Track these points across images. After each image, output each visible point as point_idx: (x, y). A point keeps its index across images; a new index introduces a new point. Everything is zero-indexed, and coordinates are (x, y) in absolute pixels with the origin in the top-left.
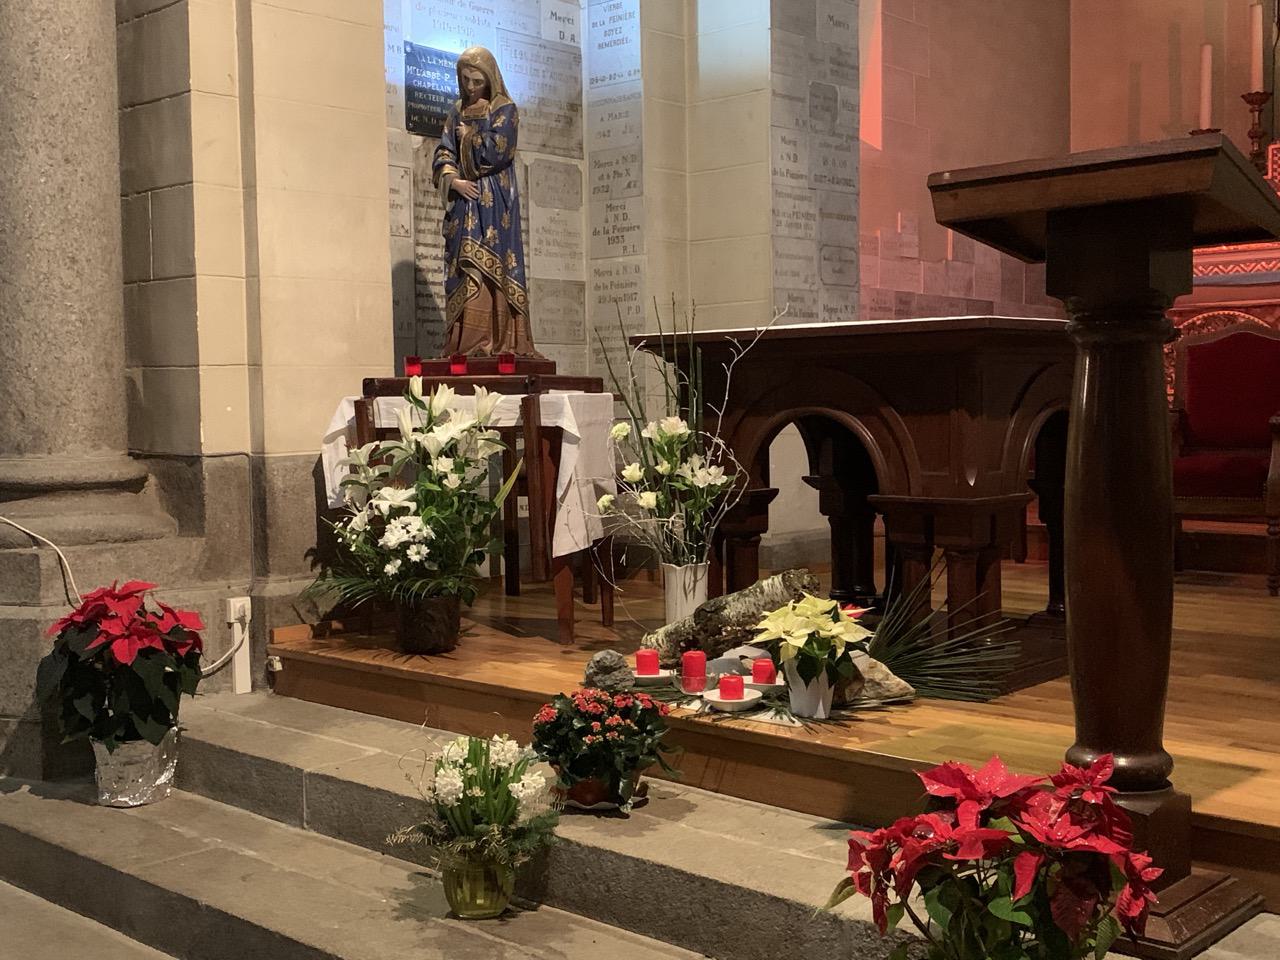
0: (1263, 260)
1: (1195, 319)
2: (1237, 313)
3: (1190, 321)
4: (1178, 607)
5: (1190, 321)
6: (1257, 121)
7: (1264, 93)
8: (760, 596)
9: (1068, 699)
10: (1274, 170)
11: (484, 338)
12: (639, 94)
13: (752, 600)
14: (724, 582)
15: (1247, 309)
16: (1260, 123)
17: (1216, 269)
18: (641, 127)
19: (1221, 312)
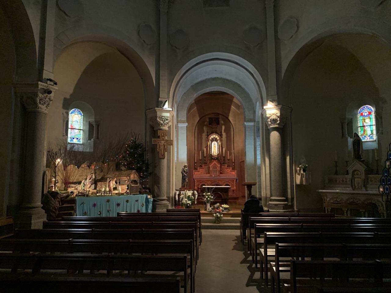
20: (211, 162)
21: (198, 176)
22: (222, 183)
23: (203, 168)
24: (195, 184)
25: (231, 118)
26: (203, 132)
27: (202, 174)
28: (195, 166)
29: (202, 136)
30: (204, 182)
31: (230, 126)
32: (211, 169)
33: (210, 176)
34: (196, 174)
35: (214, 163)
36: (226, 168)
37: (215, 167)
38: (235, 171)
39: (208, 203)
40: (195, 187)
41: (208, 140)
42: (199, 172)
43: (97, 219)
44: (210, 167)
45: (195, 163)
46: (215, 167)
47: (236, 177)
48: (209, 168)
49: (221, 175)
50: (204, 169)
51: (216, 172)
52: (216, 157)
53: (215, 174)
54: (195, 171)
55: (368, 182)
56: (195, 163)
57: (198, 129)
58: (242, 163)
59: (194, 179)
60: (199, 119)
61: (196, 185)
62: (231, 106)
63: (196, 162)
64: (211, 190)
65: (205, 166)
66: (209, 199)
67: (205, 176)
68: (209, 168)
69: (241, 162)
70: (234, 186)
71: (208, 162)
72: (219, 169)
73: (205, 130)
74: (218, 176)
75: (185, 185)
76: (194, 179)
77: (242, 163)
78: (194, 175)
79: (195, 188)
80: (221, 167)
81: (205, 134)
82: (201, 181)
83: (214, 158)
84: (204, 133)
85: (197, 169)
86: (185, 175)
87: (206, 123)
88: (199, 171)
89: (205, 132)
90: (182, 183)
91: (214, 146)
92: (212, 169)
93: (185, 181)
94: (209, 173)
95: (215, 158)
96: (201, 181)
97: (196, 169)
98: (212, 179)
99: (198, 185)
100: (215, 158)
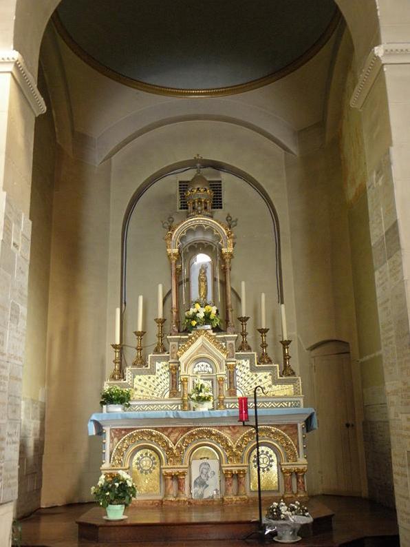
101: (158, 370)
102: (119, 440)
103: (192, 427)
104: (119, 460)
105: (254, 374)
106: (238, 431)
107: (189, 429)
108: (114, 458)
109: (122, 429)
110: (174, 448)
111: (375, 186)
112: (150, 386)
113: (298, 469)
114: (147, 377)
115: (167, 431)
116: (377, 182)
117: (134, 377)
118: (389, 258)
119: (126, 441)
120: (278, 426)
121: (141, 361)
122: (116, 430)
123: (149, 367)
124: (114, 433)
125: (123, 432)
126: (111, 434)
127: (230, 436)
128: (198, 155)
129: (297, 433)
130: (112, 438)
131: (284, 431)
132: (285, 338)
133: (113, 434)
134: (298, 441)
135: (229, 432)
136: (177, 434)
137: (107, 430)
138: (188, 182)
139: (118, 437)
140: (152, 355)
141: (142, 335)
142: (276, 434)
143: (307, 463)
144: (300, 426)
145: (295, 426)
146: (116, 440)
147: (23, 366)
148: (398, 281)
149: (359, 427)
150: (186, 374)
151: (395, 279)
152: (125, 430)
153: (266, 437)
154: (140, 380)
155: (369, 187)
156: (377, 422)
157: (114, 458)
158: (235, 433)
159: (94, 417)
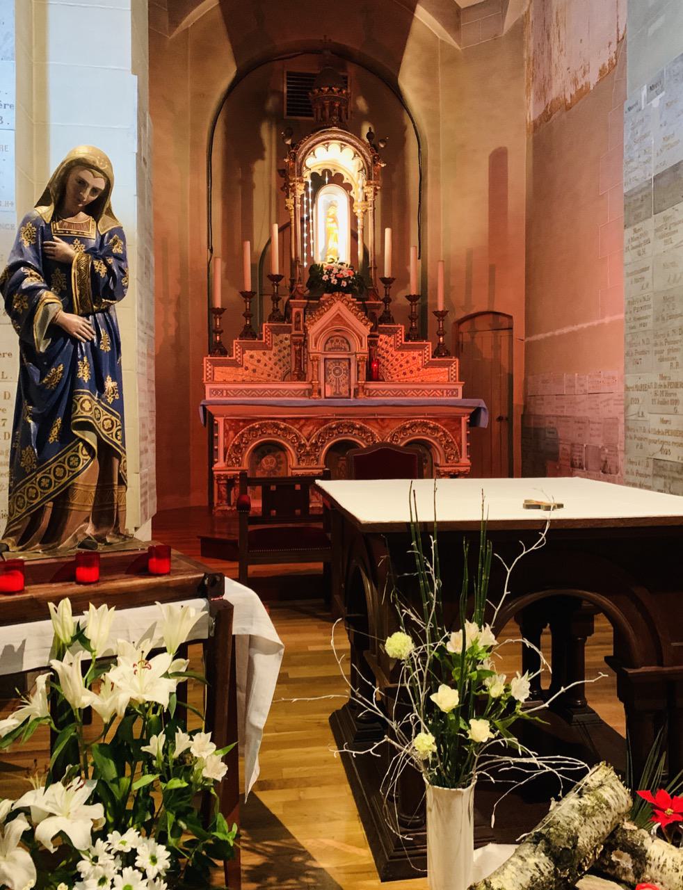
0: (269, 389)
1: (254, 424)
2: (279, 422)
3: (251, 426)
4: (588, 650)
5: (251, 426)
6: (248, 307)
7: (251, 292)
8: (607, 812)
9: (321, 742)
10: (266, 338)
11: (87, 520)
12: (13, 226)
13: (600, 818)
14: (360, 782)
15: (284, 420)
16: (249, 309)
17: (412, 392)
18: (660, 212)
19: (270, 421)
20: (313, 309)
21: (237, 392)
22: (389, 431)
23: (265, 347)
24: (212, 440)
25: (410, 83)
26: (259, 153)
27: (259, 382)
28: (212, 331)
29: (248, 172)
30: (277, 426)
31: (404, 128)
32: (315, 348)
33: (310, 392)
34: (218, 377)
35: (329, 315)
36: (401, 348)
37: (338, 336)
38: (448, 364)
39: (452, 779)
40: (212, 463)
41: (286, 188)
42: (240, 370)
43: (207, 420)
44: (306, 335)
45: (213, 312)
46: (338, 336)
47: (460, 396)
48: (301, 344)
49: (372, 386)
50: (270, 353)
51: (343, 366)
52: (345, 273)
53: (338, 381)
54: (215, 364)
55: (553, 428)
56: (213, 312)
57: (227, 123)
58: (465, 327)
59: (205, 410)
60: (231, 72)
61: (220, 447)
62: (413, 10)
63: (218, 304)
64: (497, 571)
65: (277, 331)
66: (480, 730)
67: (276, 393)
68: (304, 344)
69: (460, 322)
70: (458, 454)
71: (295, 310)
72: (360, 348)
73: (266, 144)
74: (356, 392)
75: (63, 500)
76: (205, 410)
77: (464, 324)
78: (208, 387)
79: (216, 466)
80: (372, 343)
81: (266, 162)
82: (254, 420)
83: (334, 281)
84: (263, 158)
85: (224, 352)
86: (57, 331)
87: (270, 104)
88: (235, 364)
89: (267, 154)
90: (18, 472)
91: (327, 215)
92: (320, 348)
93: (67, 437)
94: (301, 376)
95: (339, 280)
96: (254, 420)
97: (218, 350)
98: (328, 413)
99: (237, 448)
100: (339, 280)
101: (402, 355)
102: (236, 434)
103: (330, 419)
104: (236, 458)
105: (400, 353)
106: (387, 426)
107: (327, 421)
108: (230, 455)
109: (240, 420)
110: (308, 444)
111: (643, 108)
112: (265, 365)
113: (459, 472)
114: (261, 352)
115: (298, 423)
116: (649, 100)
117: (244, 352)
118: (655, 214)
119: (245, 436)
120: (436, 420)
121: (250, 333)
122: (232, 420)
123: (264, 341)
124: (230, 425)
125: (241, 424)
126: (225, 426)
127: (377, 431)
128: (325, 36)
129: (459, 429)
130: (226, 431)
131: (445, 425)
132: (440, 308)
133: (227, 426)
134: (461, 440)
135: (376, 426)
136: (311, 428)
137: (220, 421)
138: (314, 75)
139: (234, 430)
140: (267, 324)
141: (252, 297)
142: (435, 429)
143: (470, 464)
144: (465, 420)
145: (458, 420)
146: (231, 433)
147: (627, 388)
148: (670, 246)
149: (517, 423)
150: (317, 351)
151: (665, 241)
152: (244, 421)
153: (422, 433)
154: (252, 357)
155: (630, 109)
156: (548, 416)
157: (230, 455)
158: (383, 428)
159: (202, 403)
